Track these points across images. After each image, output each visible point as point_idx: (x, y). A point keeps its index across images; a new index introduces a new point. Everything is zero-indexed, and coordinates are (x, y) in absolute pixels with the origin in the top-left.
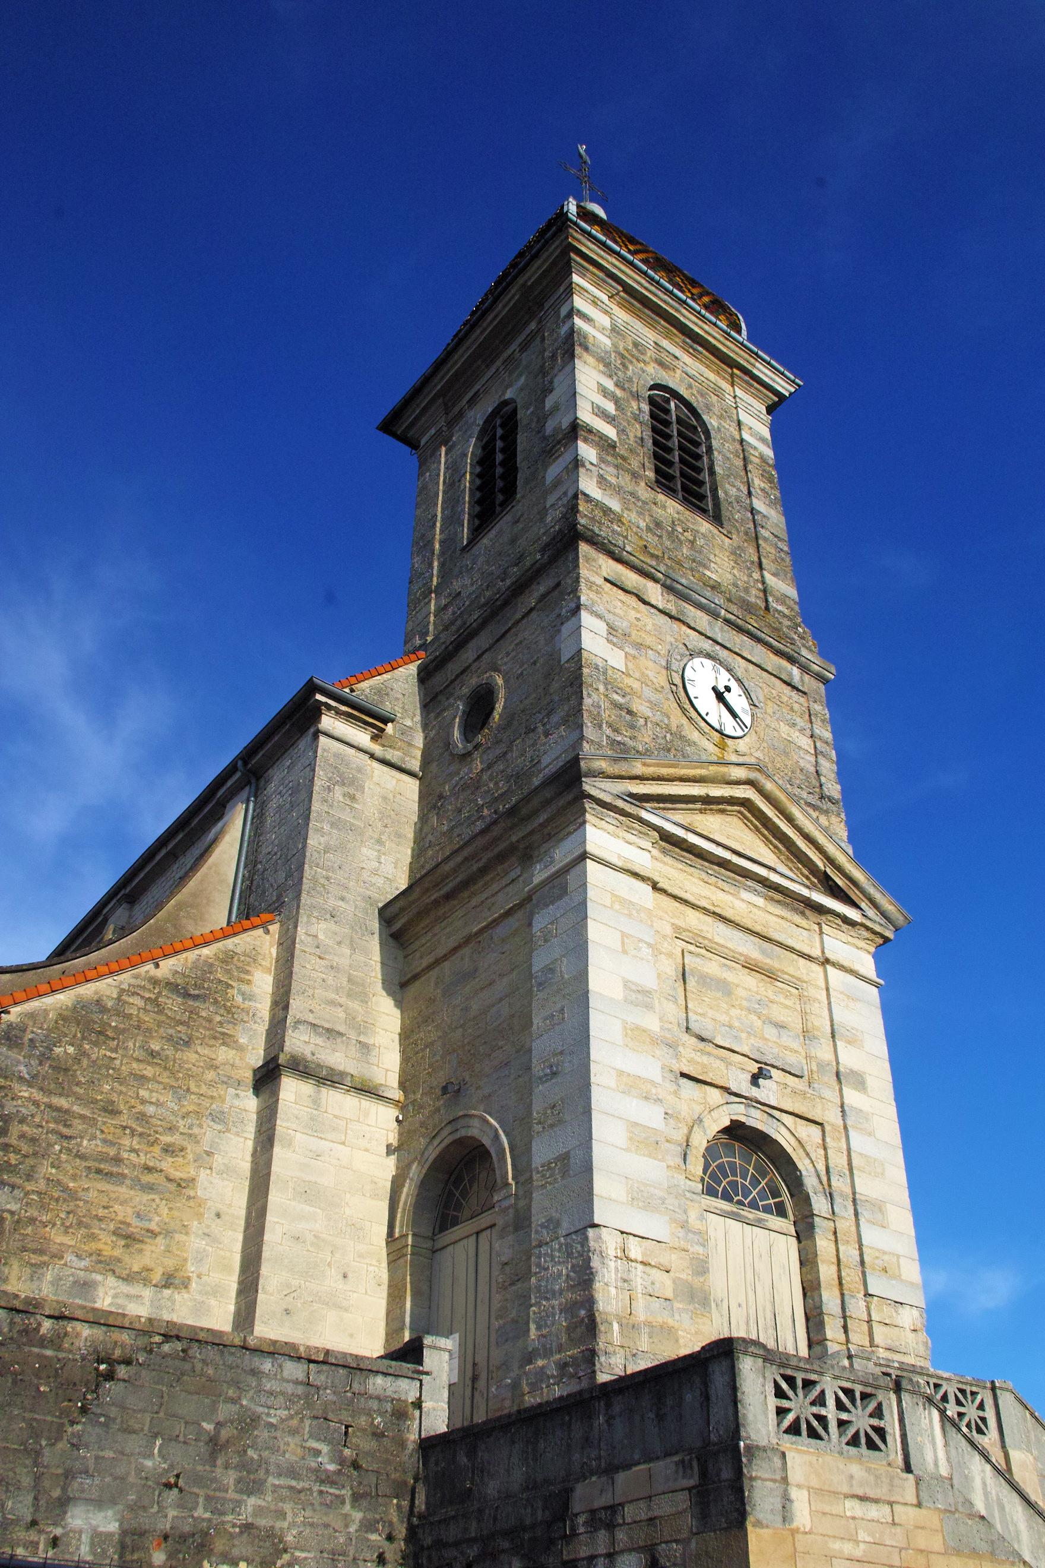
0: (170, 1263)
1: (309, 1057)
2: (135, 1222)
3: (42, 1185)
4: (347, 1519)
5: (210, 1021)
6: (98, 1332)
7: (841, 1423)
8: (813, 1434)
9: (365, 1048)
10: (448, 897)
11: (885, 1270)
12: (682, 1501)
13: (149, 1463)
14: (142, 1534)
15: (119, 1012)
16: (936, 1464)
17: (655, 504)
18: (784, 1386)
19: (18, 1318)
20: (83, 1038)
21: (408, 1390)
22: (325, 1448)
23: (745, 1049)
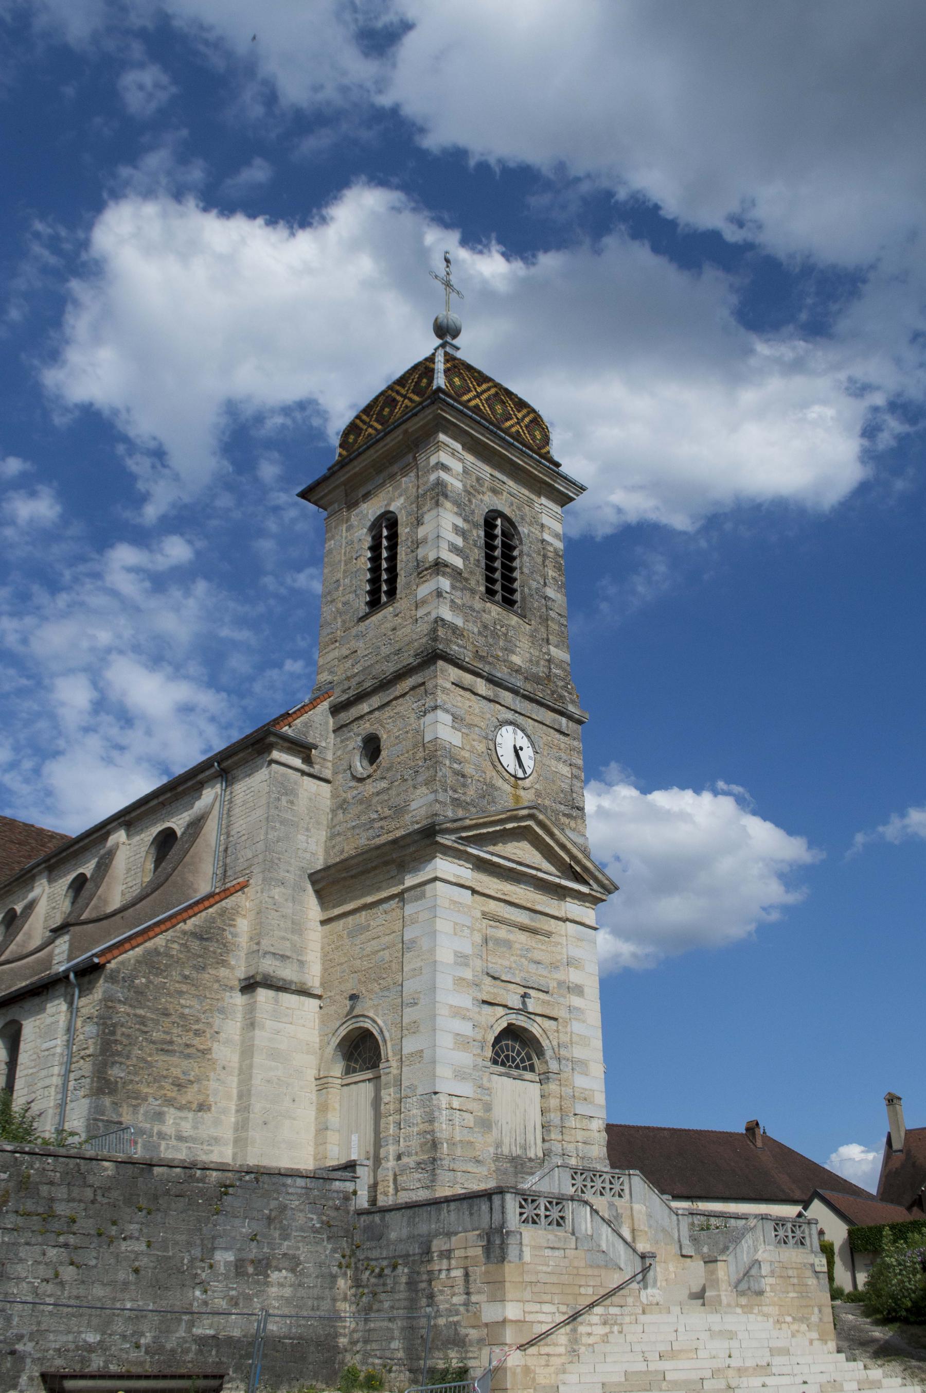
0: (201, 1098)
1: (272, 974)
2: (181, 1076)
3: (134, 1061)
4: (325, 1249)
5: (214, 953)
6: (219, 1173)
7: (546, 1216)
8: (534, 1222)
9: (301, 963)
10: (352, 877)
11: (586, 1099)
12: (479, 1251)
13: (244, 1230)
14: (243, 1260)
15: (168, 955)
16: (586, 1230)
17: (484, 611)
18: (523, 1203)
19: (187, 1171)
20: (150, 972)
21: (349, 1186)
22: (315, 1217)
23: (518, 980)
